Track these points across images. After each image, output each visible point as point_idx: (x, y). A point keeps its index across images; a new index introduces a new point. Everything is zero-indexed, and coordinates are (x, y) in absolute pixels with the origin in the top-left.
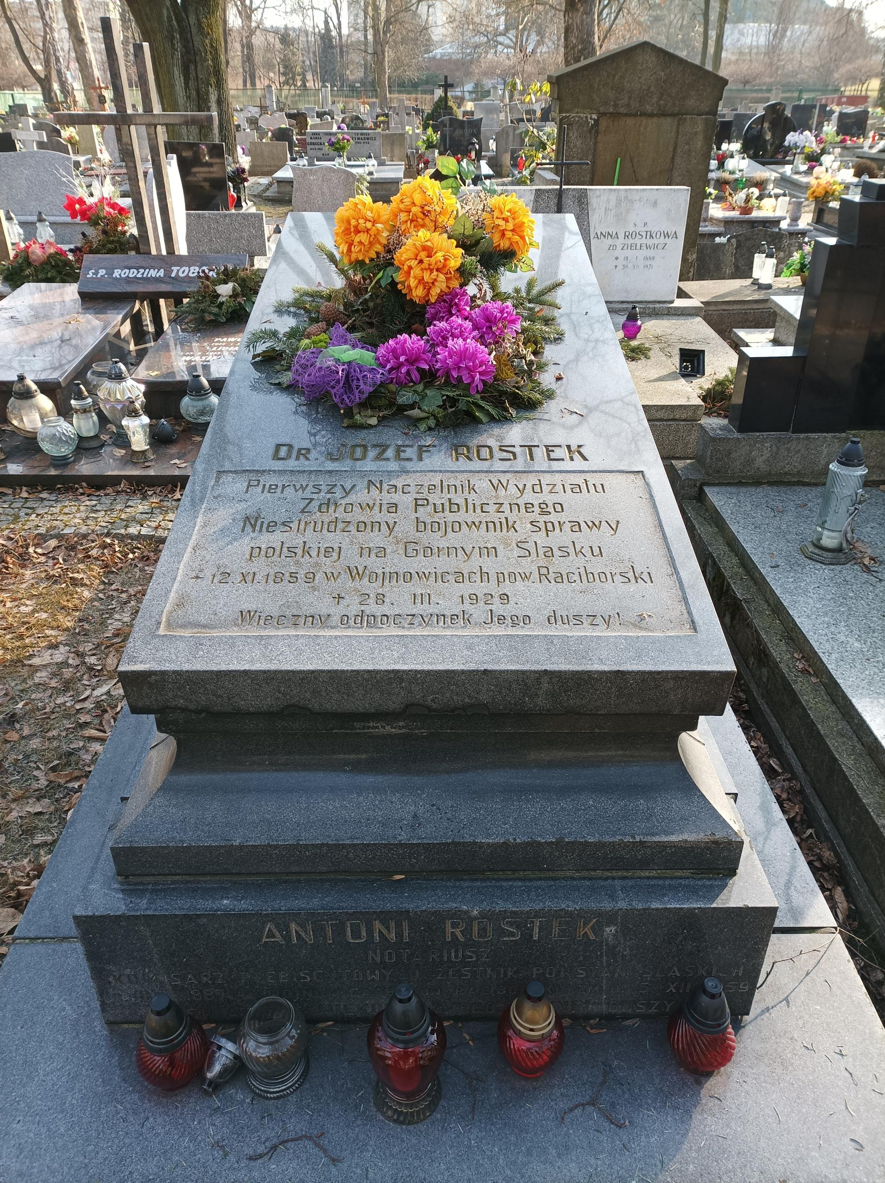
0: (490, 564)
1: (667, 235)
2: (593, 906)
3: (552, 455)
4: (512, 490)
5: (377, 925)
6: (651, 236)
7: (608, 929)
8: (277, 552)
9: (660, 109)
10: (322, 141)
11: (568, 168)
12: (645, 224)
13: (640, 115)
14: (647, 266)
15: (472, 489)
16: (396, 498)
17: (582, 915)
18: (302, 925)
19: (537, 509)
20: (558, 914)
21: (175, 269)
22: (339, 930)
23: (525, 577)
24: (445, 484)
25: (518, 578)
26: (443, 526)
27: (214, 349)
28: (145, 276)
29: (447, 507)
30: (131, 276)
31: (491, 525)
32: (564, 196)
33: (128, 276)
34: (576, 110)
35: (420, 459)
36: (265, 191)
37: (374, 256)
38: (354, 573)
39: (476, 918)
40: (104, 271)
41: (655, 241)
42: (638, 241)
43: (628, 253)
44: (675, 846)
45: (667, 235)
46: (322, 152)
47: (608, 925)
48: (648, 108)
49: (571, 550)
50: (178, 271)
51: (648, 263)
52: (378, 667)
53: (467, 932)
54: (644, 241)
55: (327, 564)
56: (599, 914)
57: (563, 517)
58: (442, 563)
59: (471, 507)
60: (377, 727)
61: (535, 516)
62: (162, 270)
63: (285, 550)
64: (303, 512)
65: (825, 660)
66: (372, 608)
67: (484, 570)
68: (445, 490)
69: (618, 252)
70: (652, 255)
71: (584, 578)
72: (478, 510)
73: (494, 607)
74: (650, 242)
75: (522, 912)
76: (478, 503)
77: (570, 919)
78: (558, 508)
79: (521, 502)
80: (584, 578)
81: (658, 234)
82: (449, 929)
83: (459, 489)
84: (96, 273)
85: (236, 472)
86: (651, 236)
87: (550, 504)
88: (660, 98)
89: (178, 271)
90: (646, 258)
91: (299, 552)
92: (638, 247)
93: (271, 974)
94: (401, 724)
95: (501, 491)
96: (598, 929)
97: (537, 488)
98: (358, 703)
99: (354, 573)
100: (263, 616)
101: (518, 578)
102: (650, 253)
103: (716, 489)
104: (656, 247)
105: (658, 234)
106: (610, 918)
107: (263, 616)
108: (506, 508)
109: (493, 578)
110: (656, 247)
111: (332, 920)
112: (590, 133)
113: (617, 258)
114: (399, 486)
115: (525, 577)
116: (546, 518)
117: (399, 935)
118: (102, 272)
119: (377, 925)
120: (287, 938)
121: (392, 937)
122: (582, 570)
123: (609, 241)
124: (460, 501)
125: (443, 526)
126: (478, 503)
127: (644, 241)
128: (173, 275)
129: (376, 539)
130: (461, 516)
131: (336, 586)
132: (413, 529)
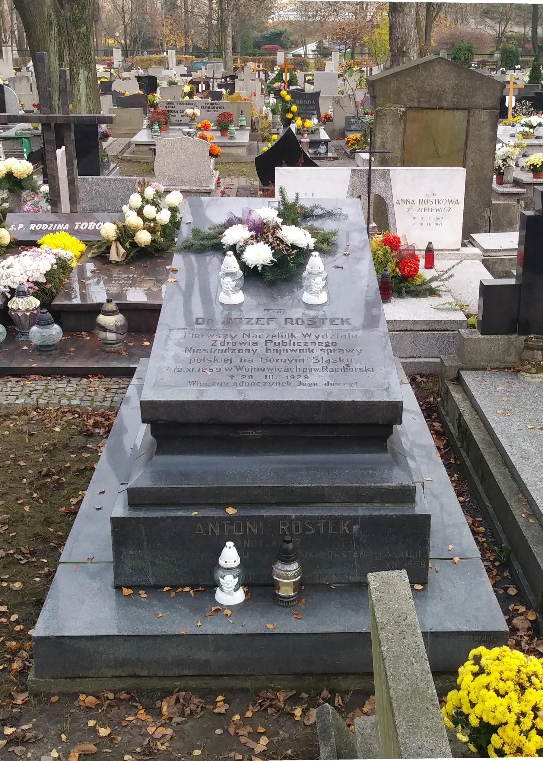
0: (300, 365)
1: (451, 202)
2: (346, 513)
3: (334, 323)
4: (313, 337)
5: (249, 525)
6: (439, 202)
7: (354, 527)
8: (203, 360)
9: (454, 105)
10: (176, 109)
13: (439, 109)
15: (293, 336)
16: (257, 340)
17: (343, 518)
18: (214, 525)
19: (324, 344)
20: (331, 517)
21: (77, 224)
23: (316, 370)
24: (280, 334)
25: (313, 370)
26: (279, 351)
27: (113, 282)
28: (54, 229)
29: (281, 343)
30: (43, 228)
31: (302, 351)
32: (372, 174)
33: (41, 229)
34: (388, 105)
35: (268, 323)
36: (123, 152)
38: (239, 368)
39: (294, 520)
40: (23, 225)
42: (430, 206)
43: (422, 214)
45: (451, 202)
46: (176, 118)
47: (354, 525)
48: (445, 104)
49: (338, 360)
50: (80, 225)
51: (439, 221)
53: (289, 529)
54: (434, 206)
55: (226, 365)
56: (349, 517)
57: (336, 348)
58: (279, 365)
59: (292, 343)
60: (249, 433)
61: (323, 347)
62: (67, 225)
63: (206, 359)
64: (213, 345)
65: (511, 458)
66: (247, 380)
67: (298, 367)
68: (280, 337)
70: (440, 216)
71: (343, 370)
72: (296, 344)
73: (301, 380)
74: (438, 206)
75: (315, 516)
76: (296, 342)
77: (337, 520)
78: (334, 344)
79: (317, 342)
80: (343, 370)
82: (282, 527)
83: (287, 336)
84: (17, 226)
85: (179, 329)
86: (439, 202)
87: (330, 343)
88: (454, 97)
89: (80, 225)
90: (436, 218)
91: (213, 360)
92: (430, 210)
94: (260, 431)
95: (307, 338)
96: (350, 527)
97: (325, 336)
98: (243, 418)
99: (239, 368)
100: (199, 383)
101: (313, 370)
102: (439, 214)
103: (468, 372)
104: (443, 210)
106: (354, 520)
107: (199, 383)
108: (309, 344)
109: (302, 370)
110: (443, 210)
111: (228, 521)
114: (258, 335)
115: (316, 370)
116: (328, 348)
117: (259, 530)
118: (21, 226)
119: (249, 525)
120: (206, 531)
121: (254, 531)
122: (342, 368)
124: (288, 341)
125: (279, 351)
126: (296, 342)
127: (434, 206)
128: (76, 228)
129: (248, 356)
130: (288, 347)
131: (231, 373)
132: (265, 351)
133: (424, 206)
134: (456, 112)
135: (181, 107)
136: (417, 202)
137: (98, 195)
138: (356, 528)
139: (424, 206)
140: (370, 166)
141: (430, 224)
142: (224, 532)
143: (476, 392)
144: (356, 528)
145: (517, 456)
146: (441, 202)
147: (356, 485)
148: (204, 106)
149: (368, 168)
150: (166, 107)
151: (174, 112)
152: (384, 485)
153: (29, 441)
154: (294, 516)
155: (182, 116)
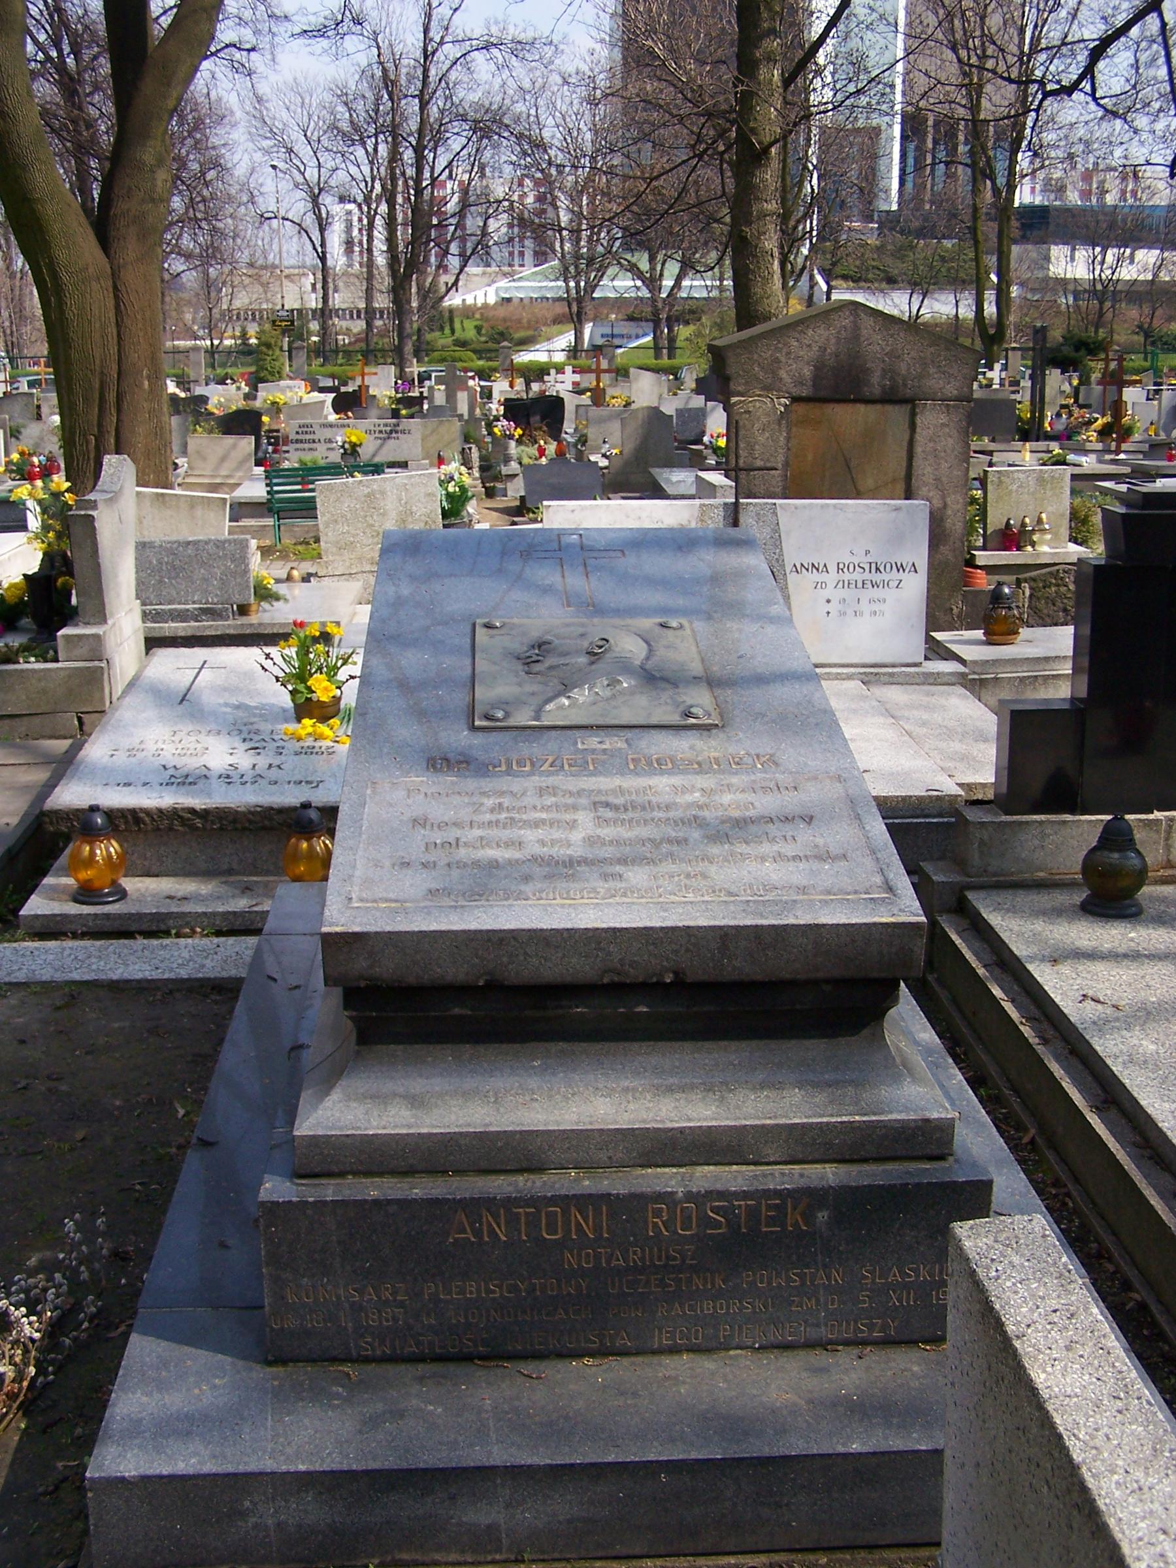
6: (877, 569)
7: (820, 1215)
10: (316, 437)
11: (748, 475)
12: (867, 552)
14: (875, 613)
22: (533, 1221)
37: (757, 482)
41: (885, 576)
44: (885, 1127)
52: (576, 926)
69: (828, 592)
74: (877, 577)
81: (888, 566)
82: (652, 1219)
86: (877, 569)
93: (457, 1287)
96: (808, 1216)
103: (982, 894)
105: (888, 566)
112: (780, 424)
113: (828, 601)
117: (597, 1228)
120: (478, 1233)
123: (815, 576)
127: (867, 576)
133: (846, 576)
134: (889, 408)
135: (328, 433)
136: (832, 568)
137: (173, 574)
138: (822, 1216)
139: (846, 576)
140: (737, 499)
141: (862, 614)
142: (520, 1233)
143: (1008, 934)
144: (822, 1216)
145: (1120, 1060)
146: (882, 569)
147: (819, 1120)
148: (372, 428)
149: (734, 500)
150: (297, 433)
151: (314, 441)
152: (882, 1118)
153: (32, 1534)
154: (681, 1194)
155: (329, 449)
